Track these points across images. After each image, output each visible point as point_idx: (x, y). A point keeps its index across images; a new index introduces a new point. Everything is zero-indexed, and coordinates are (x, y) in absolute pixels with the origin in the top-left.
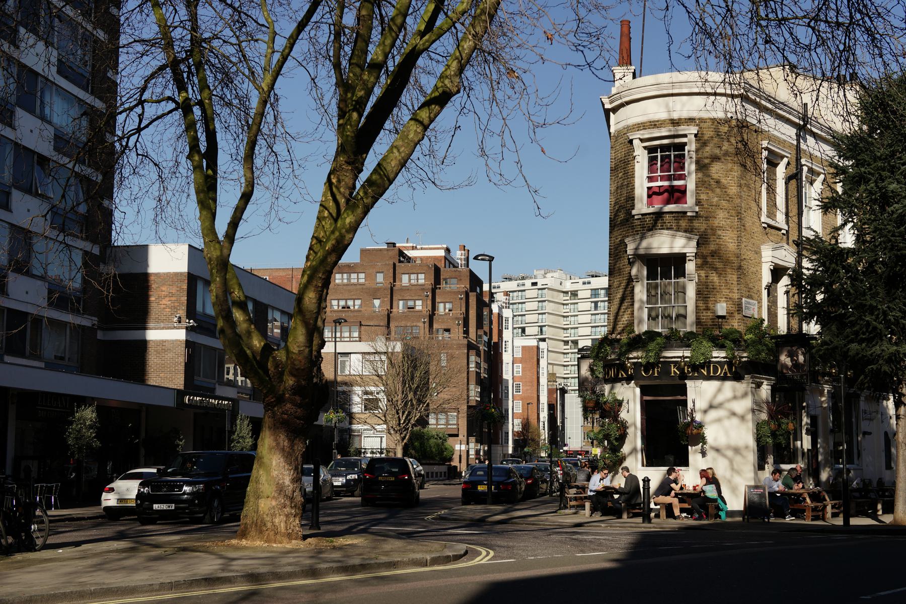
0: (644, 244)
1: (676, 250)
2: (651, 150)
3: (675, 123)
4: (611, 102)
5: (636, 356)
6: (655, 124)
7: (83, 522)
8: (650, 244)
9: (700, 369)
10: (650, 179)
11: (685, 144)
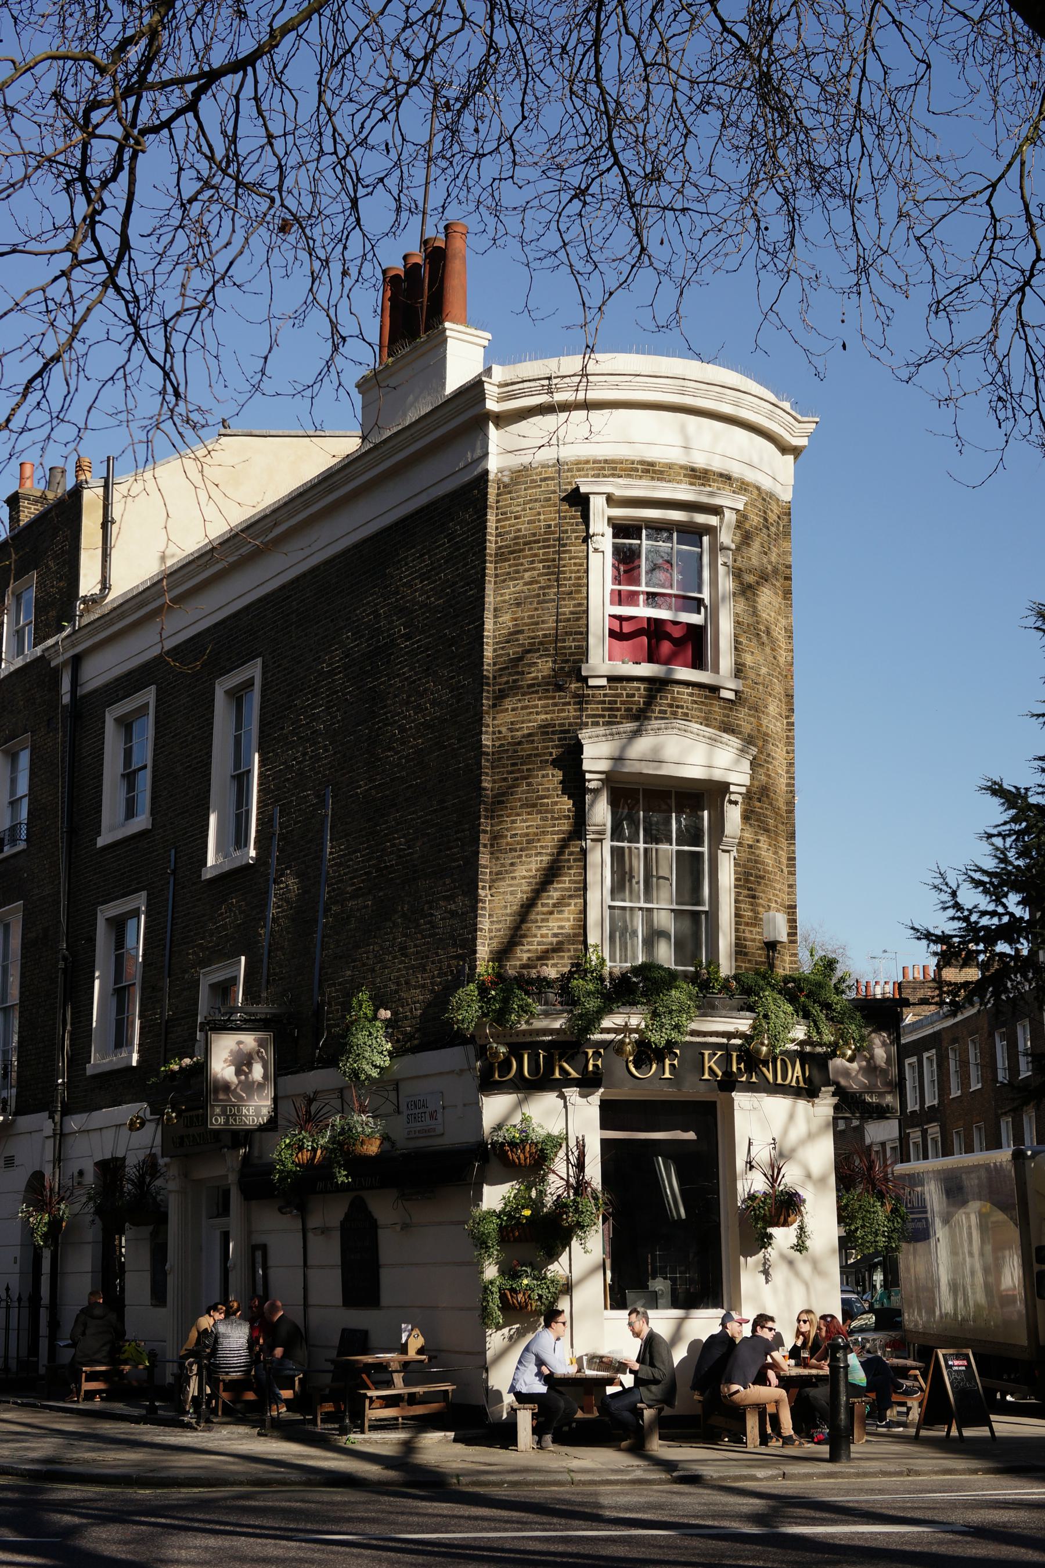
0: (642, 746)
1: (718, 775)
2: (622, 529)
3: (698, 476)
4: (501, 399)
5: (625, 1021)
6: (650, 470)
7: (462, 1521)
8: (656, 749)
9: (748, 1066)
10: (620, 598)
11: (711, 530)
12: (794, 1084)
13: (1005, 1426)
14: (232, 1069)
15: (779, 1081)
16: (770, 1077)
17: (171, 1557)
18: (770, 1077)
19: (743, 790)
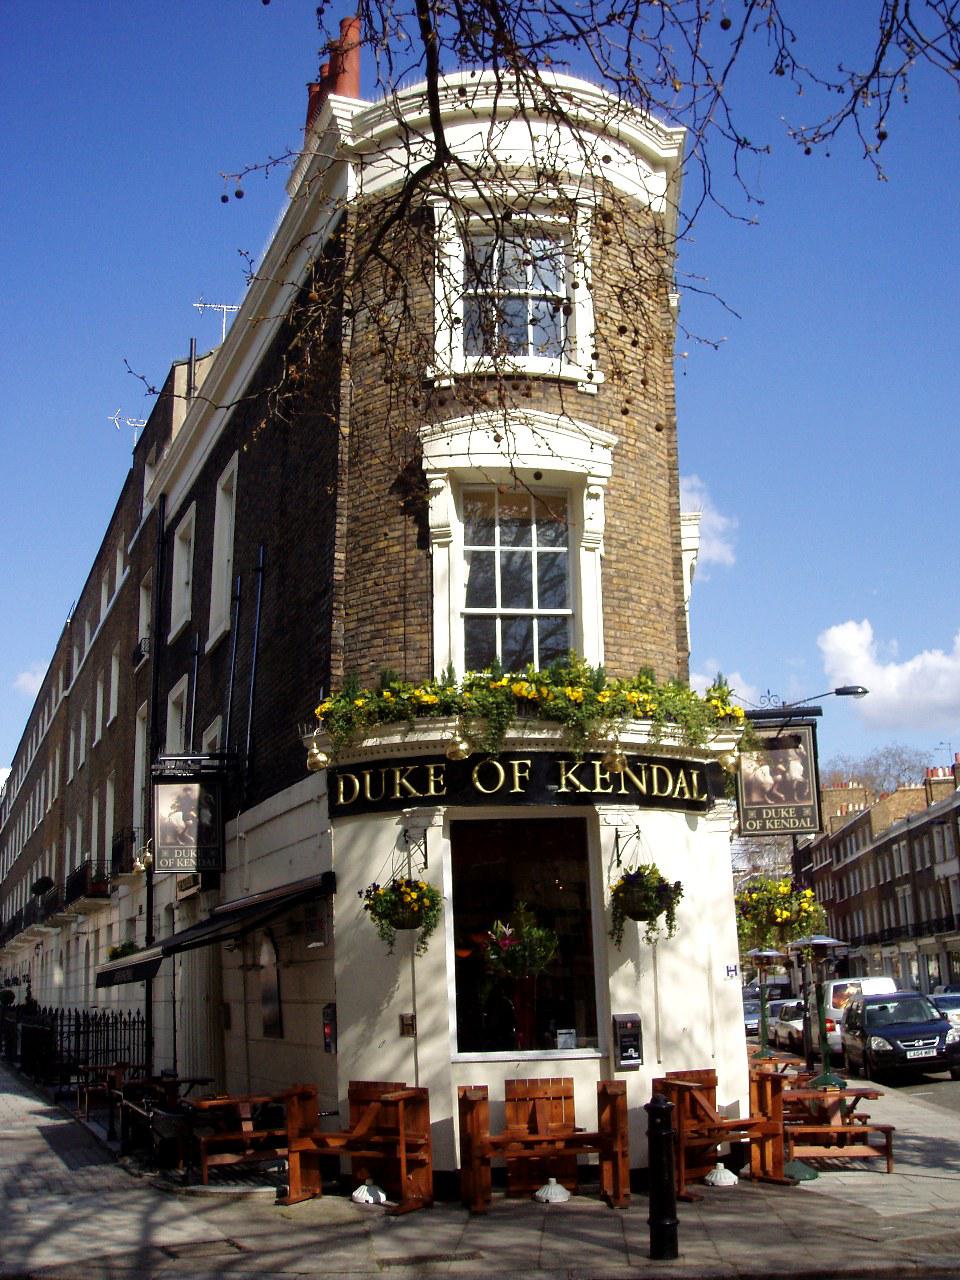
12: (676, 795)
13: (876, 1007)
14: (180, 814)
15: (656, 792)
16: (643, 788)
17: (403, 1268)
18: (643, 788)
19: (604, 482)
